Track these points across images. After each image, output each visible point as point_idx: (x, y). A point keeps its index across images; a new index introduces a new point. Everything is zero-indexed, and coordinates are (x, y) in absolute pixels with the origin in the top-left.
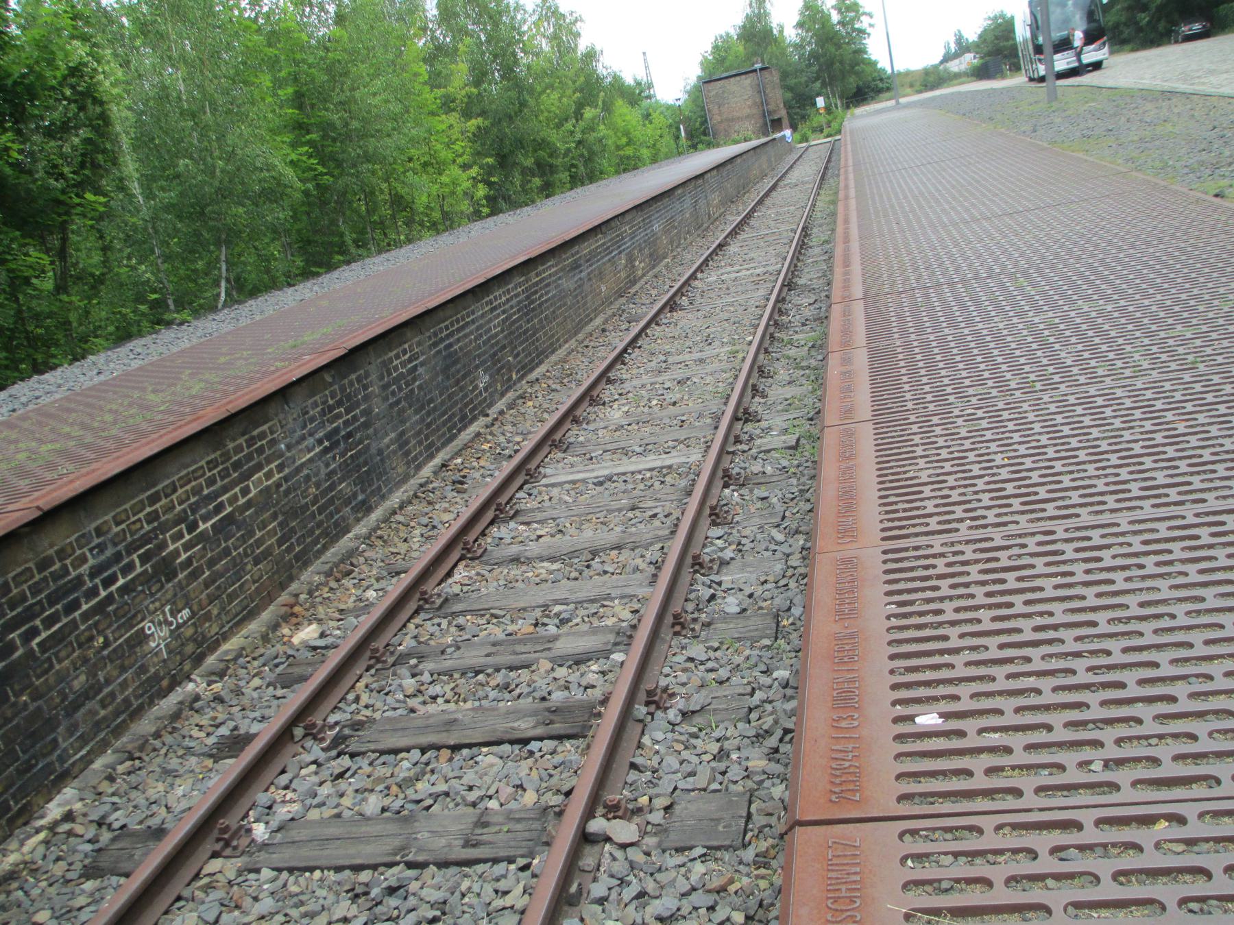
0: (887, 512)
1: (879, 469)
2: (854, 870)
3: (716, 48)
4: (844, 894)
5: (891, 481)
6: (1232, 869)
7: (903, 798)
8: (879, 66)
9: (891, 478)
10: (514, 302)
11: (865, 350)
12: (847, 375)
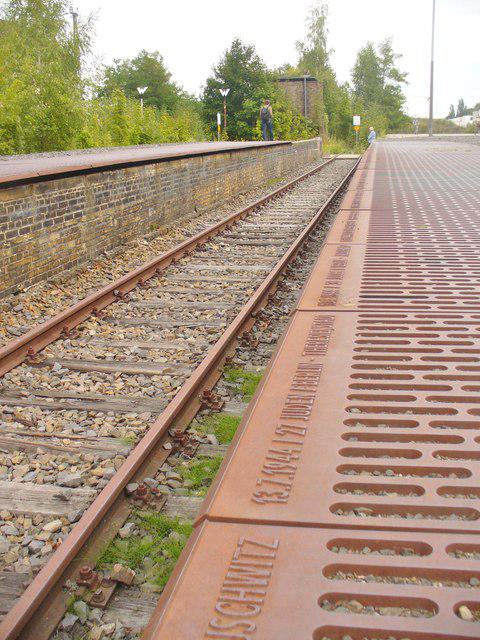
0: (362, 328)
1: (355, 376)
2: (261, 572)
3: (361, 57)
4: (241, 598)
5: (371, 350)
6: (479, 440)
7: (334, 509)
8: (171, 81)
9: (369, 346)
10: (463, 174)
11: (355, 317)
12: (307, 377)
